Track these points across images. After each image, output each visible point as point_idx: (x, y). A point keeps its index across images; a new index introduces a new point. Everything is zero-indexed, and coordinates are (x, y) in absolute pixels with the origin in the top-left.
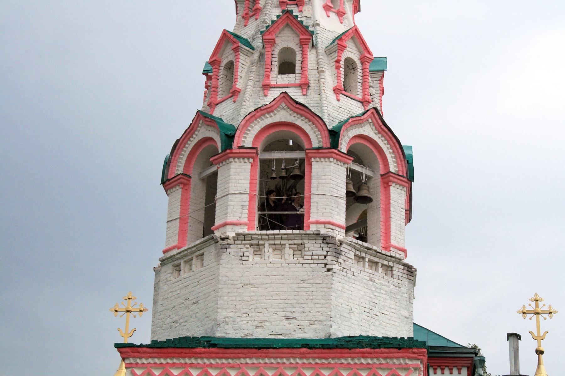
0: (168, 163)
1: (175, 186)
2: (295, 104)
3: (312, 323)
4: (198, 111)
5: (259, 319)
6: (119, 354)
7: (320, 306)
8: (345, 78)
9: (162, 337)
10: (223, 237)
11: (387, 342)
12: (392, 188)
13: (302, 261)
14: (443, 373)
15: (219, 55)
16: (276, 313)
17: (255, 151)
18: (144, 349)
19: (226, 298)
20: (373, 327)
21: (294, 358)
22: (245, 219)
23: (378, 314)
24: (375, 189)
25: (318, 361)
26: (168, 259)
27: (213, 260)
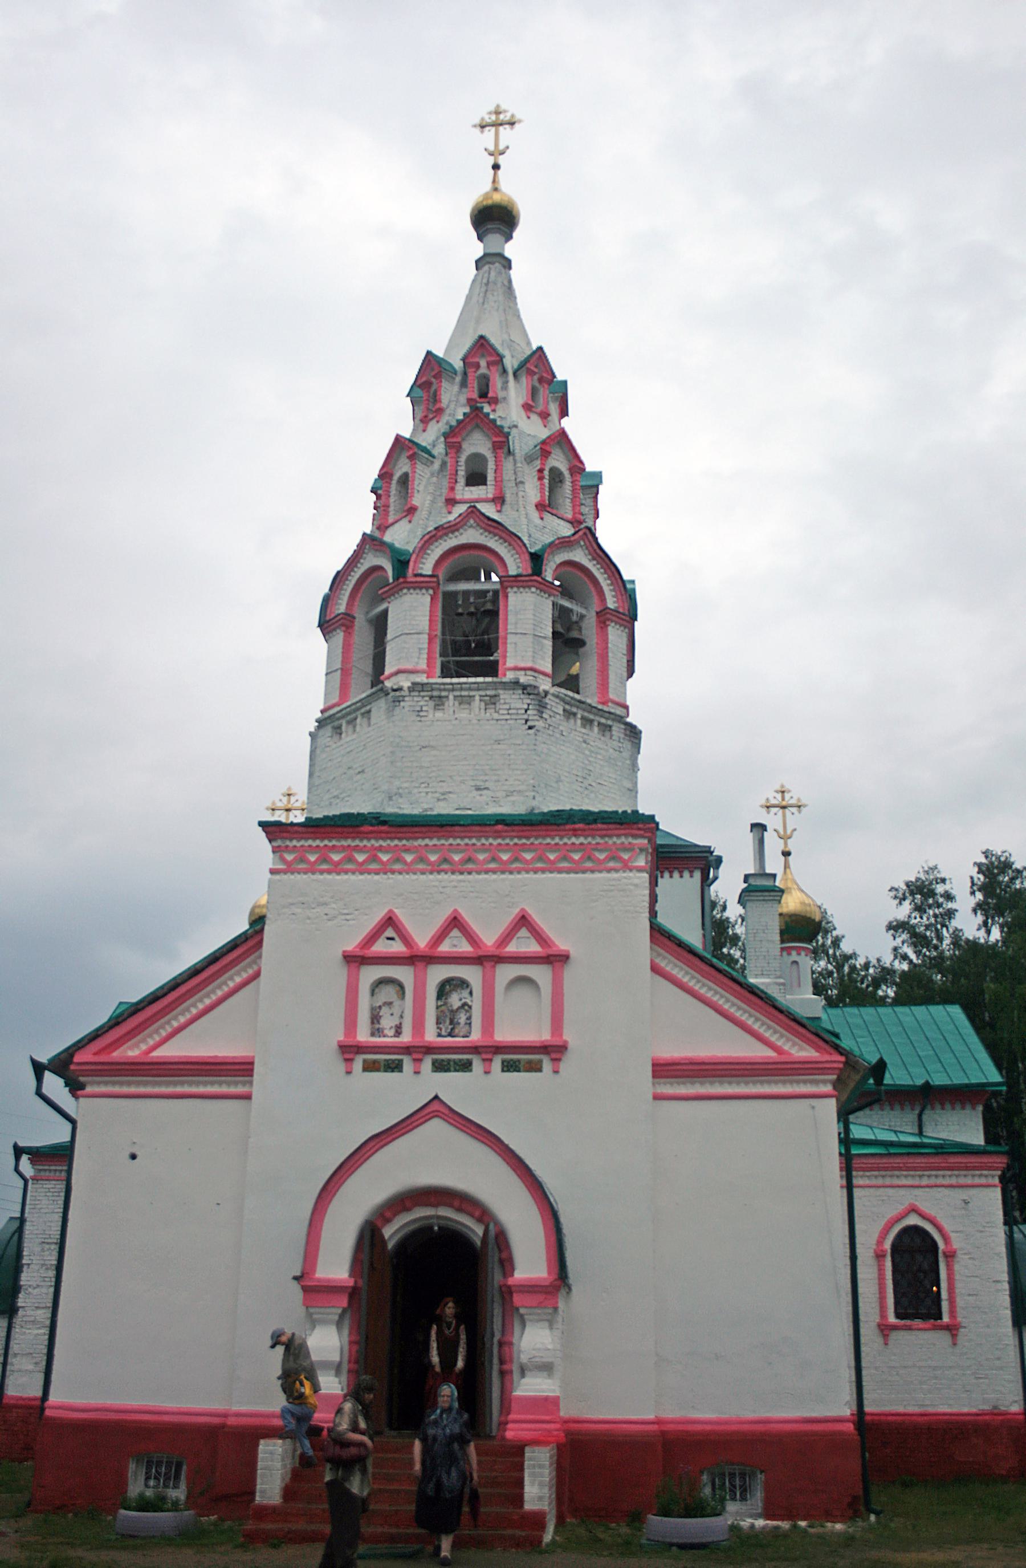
0: (327, 601)
1: (335, 629)
2: (486, 521)
3: (509, 794)
4: (364, 534)
5: (441, 790)
6: (264, 834)
7: (519, 772)
8: (550, 492)
9: (318, 814)
10: (395, 687)
11: (606, 816)
12: (610, 628)
13: (496, 716)
14: (671, 877)
15: (390, 466)
16: (463, 782)
17: (435, 579)
18: (296, 828)
19: (399, 764)
20: (587, 801)
21: (487, 838)
22: (423, 665)
23: (594, 784)
24: (589, 630)
25: (516, 840)
26: (326, 719)
27: (383, 717)
